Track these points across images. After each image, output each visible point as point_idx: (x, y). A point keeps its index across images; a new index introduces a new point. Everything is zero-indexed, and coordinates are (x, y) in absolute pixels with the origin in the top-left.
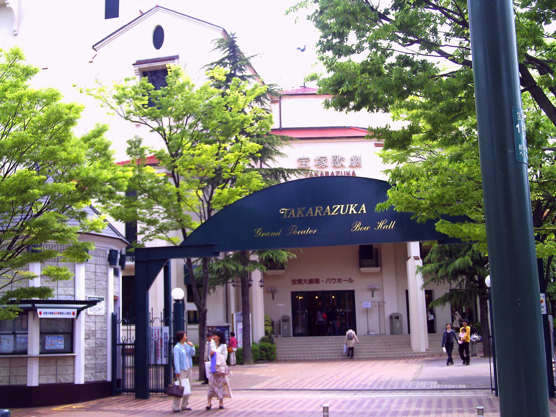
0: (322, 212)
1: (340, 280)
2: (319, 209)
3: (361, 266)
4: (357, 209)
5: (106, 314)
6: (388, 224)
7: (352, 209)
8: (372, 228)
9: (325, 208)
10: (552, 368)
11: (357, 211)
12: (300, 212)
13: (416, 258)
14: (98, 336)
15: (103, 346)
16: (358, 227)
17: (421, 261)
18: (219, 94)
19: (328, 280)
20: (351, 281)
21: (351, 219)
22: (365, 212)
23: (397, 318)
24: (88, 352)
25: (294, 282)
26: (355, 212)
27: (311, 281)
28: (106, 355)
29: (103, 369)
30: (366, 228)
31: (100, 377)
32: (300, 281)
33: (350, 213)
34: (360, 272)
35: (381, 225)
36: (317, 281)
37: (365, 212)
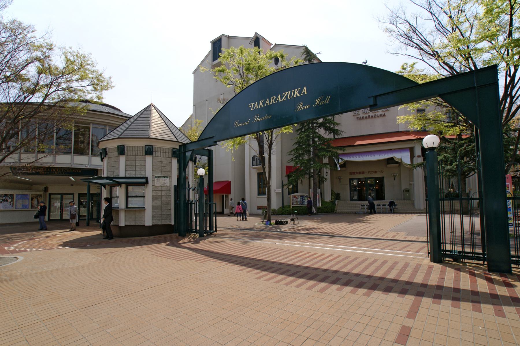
0: (275, 101)
1: (376, 172)
2: (273, 98)
3: (388, 164)
4: (300, 92)
5: (171, 186)
6: (324, 99)
7: (296, 93)
8: (311, 106)
9: (277, 97)
10: (508, 225)
11: (300, 94)
12: (261, 104)
13: (419, 157)
14: (164, 198)
15: (169, 204)
16: (300, 107)
17: (422, 158)
18: (271, 59)
19: (369, 172)
20: (382, 172)
21: (296, 101)
22: (306, 93)
23: (408, 191)
24: (154, 208)
25: (351, 174)
26: (298, 95)
27: (360, 173)
28: (170, 209)
29: (168, 217)
30: (307, 107)
31: (165, 222)
32: (354, 173)
33: (295, 96)
34: (387, 167)
35: (318, 101)
36: (363, 173)
37: (306, 93)
